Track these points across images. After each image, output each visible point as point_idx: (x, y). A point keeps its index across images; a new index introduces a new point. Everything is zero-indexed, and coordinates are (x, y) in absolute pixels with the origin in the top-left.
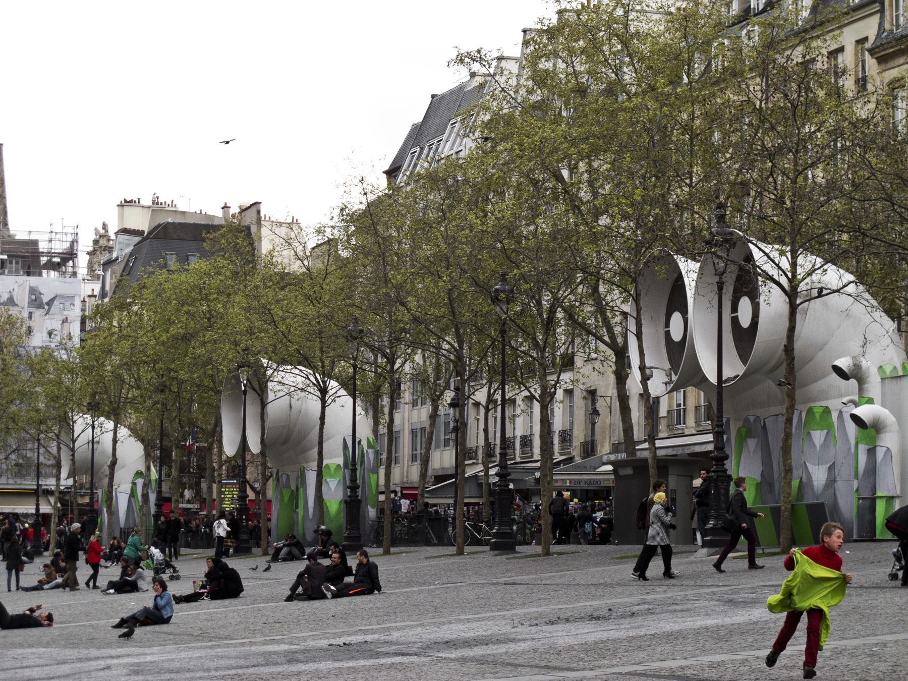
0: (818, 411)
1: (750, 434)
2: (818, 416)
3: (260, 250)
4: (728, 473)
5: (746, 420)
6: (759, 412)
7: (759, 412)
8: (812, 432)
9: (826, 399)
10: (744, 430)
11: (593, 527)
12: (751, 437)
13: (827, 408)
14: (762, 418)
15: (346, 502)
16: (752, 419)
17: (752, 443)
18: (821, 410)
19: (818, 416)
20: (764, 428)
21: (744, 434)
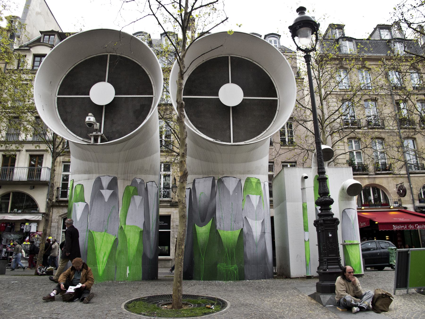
0: (254, 181)
1: (136, 192)
2: (254, 184)
3: (97, 271)
4: (334, 217)
5: (134, 182)
6: (143, 177)
7: (143, 177)
8: (250, 195)
9: (259, 174)
10: (132, 189)
11: (359, 296)
12: (137, 195)
13: (259, 180)
14: (145, 182)
15: (34, 188)
16: (139, 181)
17: (138, 199)
18: (255, 181)
19: (254, 184)
20: (146, 189)
21: (132, 192)
